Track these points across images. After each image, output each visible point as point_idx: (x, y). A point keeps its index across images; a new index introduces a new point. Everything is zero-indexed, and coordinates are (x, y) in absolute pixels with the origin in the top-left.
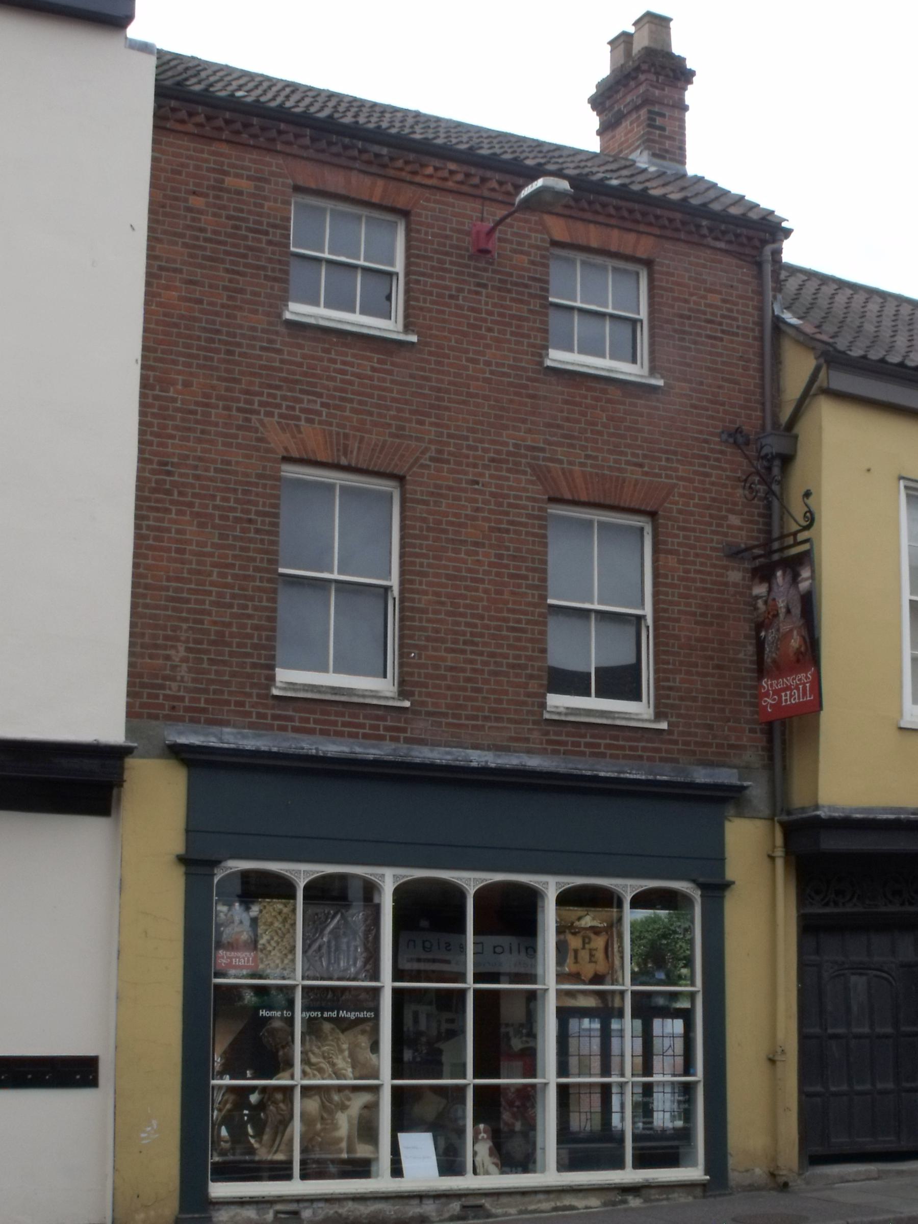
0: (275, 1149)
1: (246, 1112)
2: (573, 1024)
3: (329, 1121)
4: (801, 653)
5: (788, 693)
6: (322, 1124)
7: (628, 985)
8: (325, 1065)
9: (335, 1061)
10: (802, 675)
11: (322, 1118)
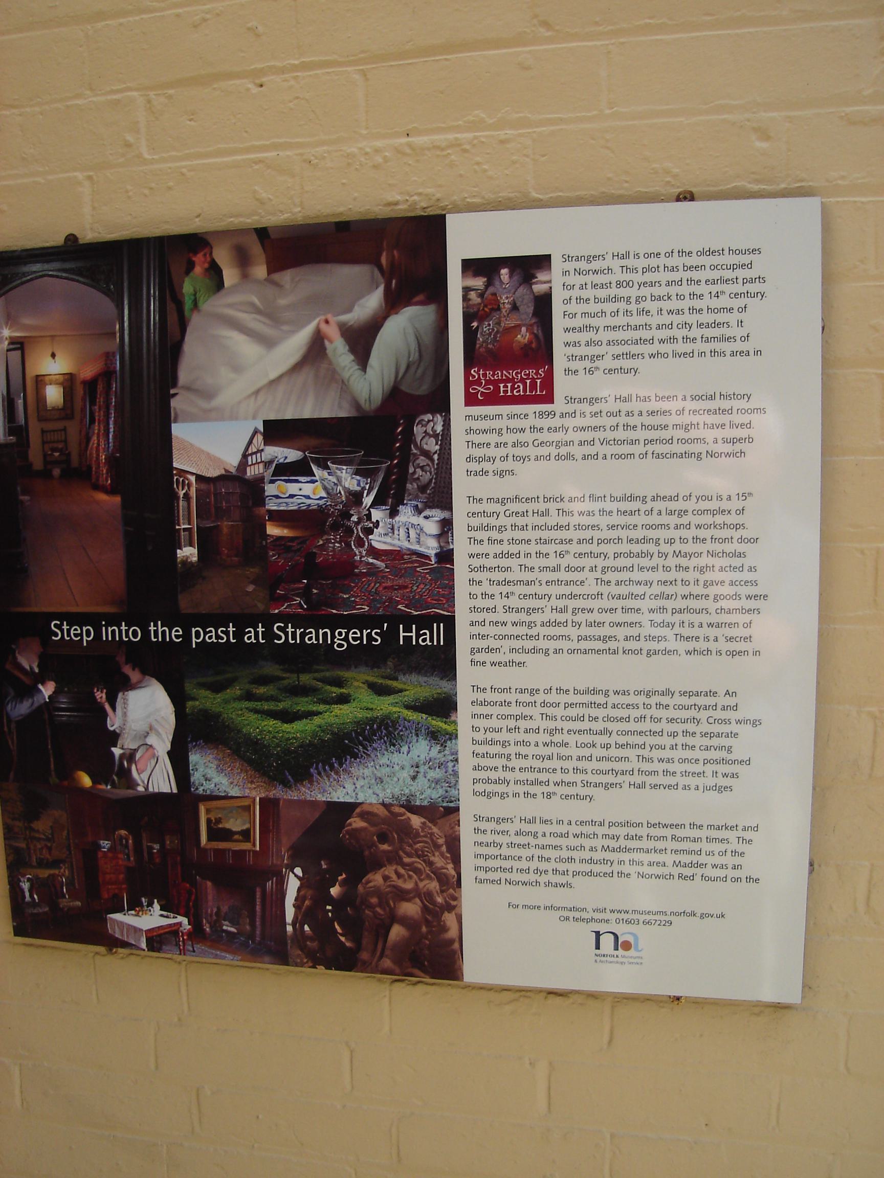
0: (378, 954)
1: (329, 907)
2: (63, 432)
3: (435, 924)
4: (531, 349)
5: (509, 385)
6: (426, 927)
7: (224, 504)
8: (420, 864)
9: (432, 858)
10: (532, 372)
11: (427, 921)
